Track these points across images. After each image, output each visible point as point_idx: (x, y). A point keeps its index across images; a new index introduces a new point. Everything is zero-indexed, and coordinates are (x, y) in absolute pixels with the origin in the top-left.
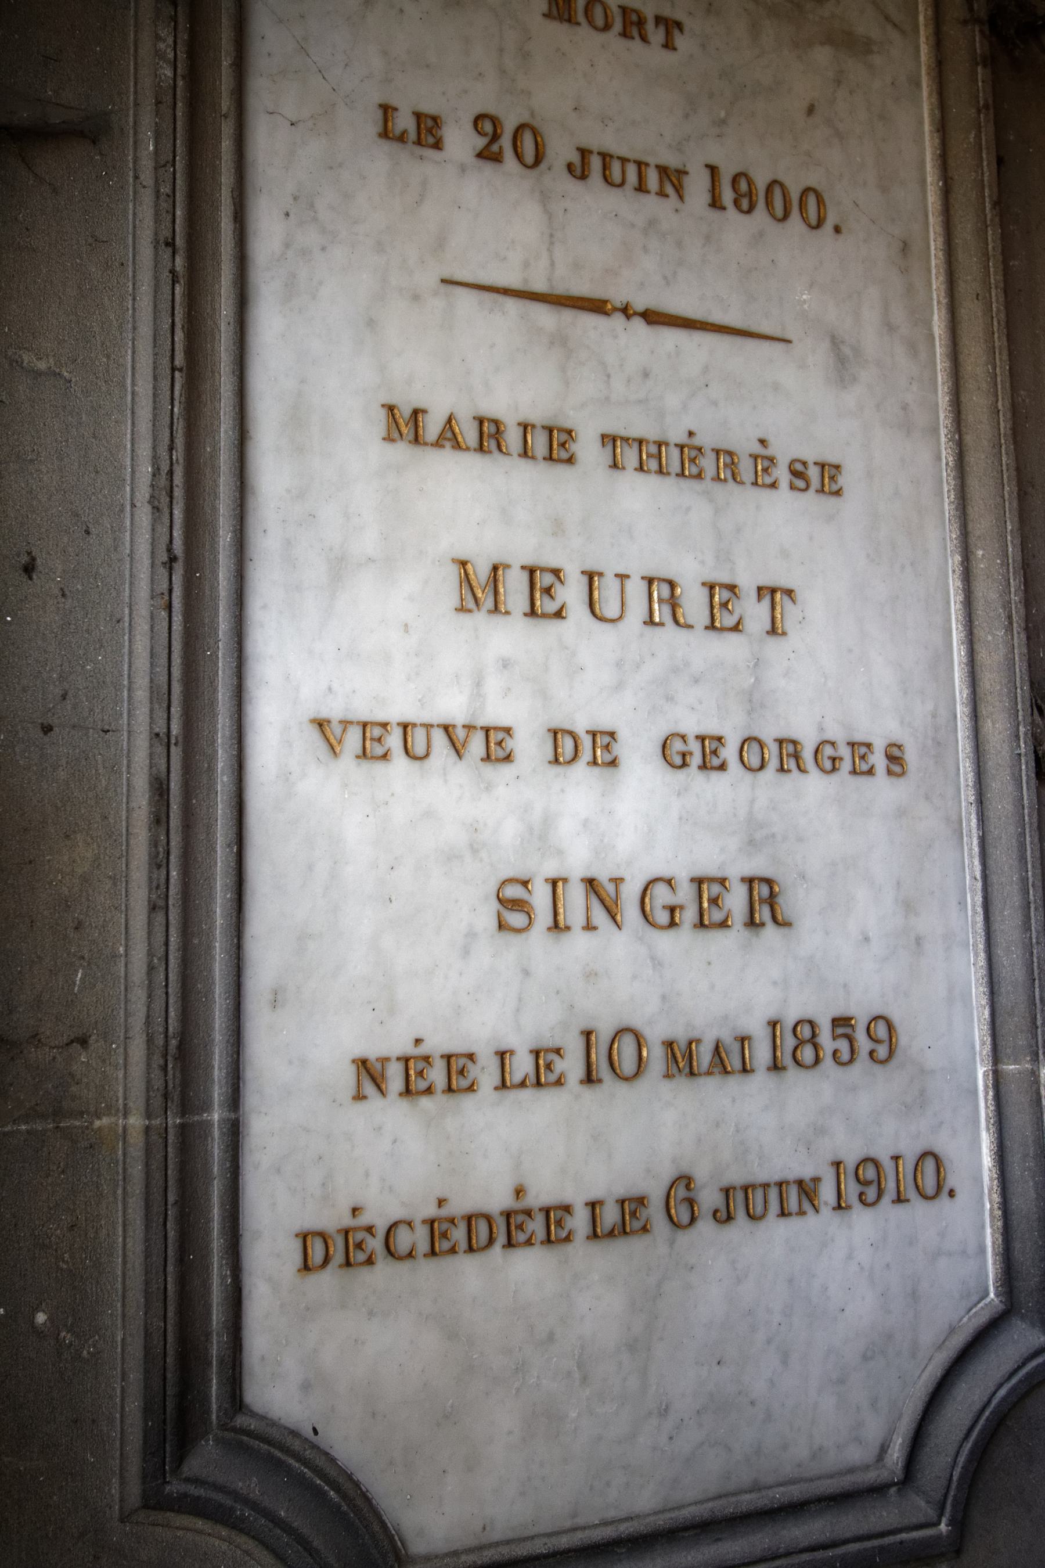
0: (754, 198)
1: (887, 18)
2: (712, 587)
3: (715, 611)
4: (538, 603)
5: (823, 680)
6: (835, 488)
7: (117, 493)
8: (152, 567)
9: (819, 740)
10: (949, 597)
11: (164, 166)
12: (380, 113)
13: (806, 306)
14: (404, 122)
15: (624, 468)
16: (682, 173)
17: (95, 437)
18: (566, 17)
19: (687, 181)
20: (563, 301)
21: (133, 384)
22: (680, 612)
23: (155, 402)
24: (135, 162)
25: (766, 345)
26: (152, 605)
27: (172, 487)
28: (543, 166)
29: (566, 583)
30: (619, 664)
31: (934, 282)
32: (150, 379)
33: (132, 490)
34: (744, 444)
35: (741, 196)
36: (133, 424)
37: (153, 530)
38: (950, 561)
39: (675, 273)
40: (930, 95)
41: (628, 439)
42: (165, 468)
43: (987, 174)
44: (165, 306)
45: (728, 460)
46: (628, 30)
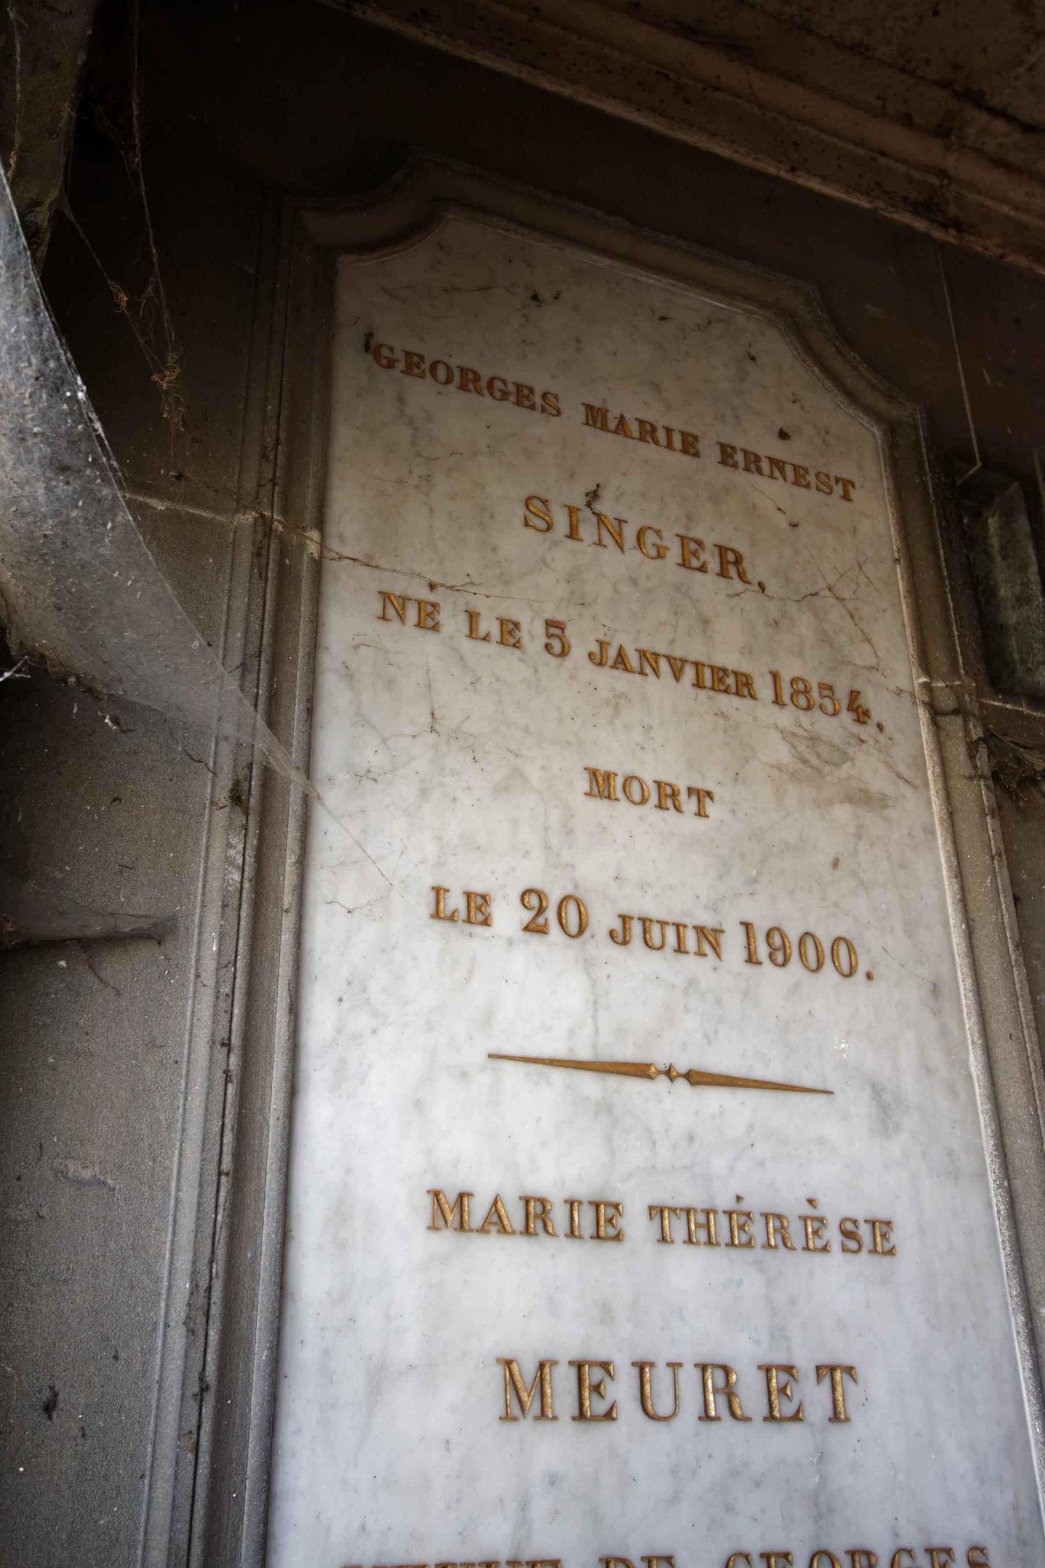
0: (788, 951)
1: (899, 776)
2: (768, 1370)
3: (773, 1397)
4: (587, 1403)
5: (892, 1473)
6: (887, 1247)
7: (151, 1310)
8: (182, 1400)
9: (894, 1548)
10: (1016, 1362)
11: (226, 966)
12: (432, 895)
13: (845, 1056)
14: (455, 902)
15: (672, 1242)
16: (718, 931)
17: (133, 1249)
18: (606, 794)
19: (723, 938)
20: (607, 1067)
21: (178, 1189)
22: (736, 1403)
23: (198, 1211)
24: (198, 961)
25: (808, 1097)
26: (178, 1447)
27: (209, 1305)
28: (587, 934)
29: (616, 1378)
30: (674, 1471)
31: (966, 1021)
32: (196, 1185)
33: (167, 1306)
34: (793, 1206)
35: (776, 950)
36: (174, 1233)
37: (186, 1356)
38: (1013, 1320)
39: (716, 1031)
40: (945, 843)
41: (676, 1209)
42: (204, 1285)
43: (1006, 917)
44: (217, 1107)
45: (778, 1224)
46: (663, 802)
